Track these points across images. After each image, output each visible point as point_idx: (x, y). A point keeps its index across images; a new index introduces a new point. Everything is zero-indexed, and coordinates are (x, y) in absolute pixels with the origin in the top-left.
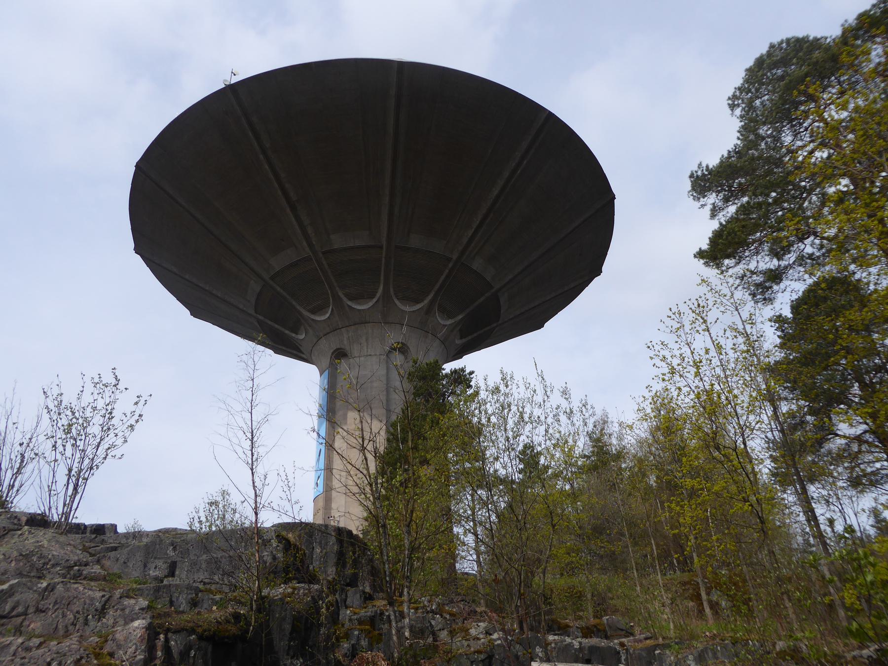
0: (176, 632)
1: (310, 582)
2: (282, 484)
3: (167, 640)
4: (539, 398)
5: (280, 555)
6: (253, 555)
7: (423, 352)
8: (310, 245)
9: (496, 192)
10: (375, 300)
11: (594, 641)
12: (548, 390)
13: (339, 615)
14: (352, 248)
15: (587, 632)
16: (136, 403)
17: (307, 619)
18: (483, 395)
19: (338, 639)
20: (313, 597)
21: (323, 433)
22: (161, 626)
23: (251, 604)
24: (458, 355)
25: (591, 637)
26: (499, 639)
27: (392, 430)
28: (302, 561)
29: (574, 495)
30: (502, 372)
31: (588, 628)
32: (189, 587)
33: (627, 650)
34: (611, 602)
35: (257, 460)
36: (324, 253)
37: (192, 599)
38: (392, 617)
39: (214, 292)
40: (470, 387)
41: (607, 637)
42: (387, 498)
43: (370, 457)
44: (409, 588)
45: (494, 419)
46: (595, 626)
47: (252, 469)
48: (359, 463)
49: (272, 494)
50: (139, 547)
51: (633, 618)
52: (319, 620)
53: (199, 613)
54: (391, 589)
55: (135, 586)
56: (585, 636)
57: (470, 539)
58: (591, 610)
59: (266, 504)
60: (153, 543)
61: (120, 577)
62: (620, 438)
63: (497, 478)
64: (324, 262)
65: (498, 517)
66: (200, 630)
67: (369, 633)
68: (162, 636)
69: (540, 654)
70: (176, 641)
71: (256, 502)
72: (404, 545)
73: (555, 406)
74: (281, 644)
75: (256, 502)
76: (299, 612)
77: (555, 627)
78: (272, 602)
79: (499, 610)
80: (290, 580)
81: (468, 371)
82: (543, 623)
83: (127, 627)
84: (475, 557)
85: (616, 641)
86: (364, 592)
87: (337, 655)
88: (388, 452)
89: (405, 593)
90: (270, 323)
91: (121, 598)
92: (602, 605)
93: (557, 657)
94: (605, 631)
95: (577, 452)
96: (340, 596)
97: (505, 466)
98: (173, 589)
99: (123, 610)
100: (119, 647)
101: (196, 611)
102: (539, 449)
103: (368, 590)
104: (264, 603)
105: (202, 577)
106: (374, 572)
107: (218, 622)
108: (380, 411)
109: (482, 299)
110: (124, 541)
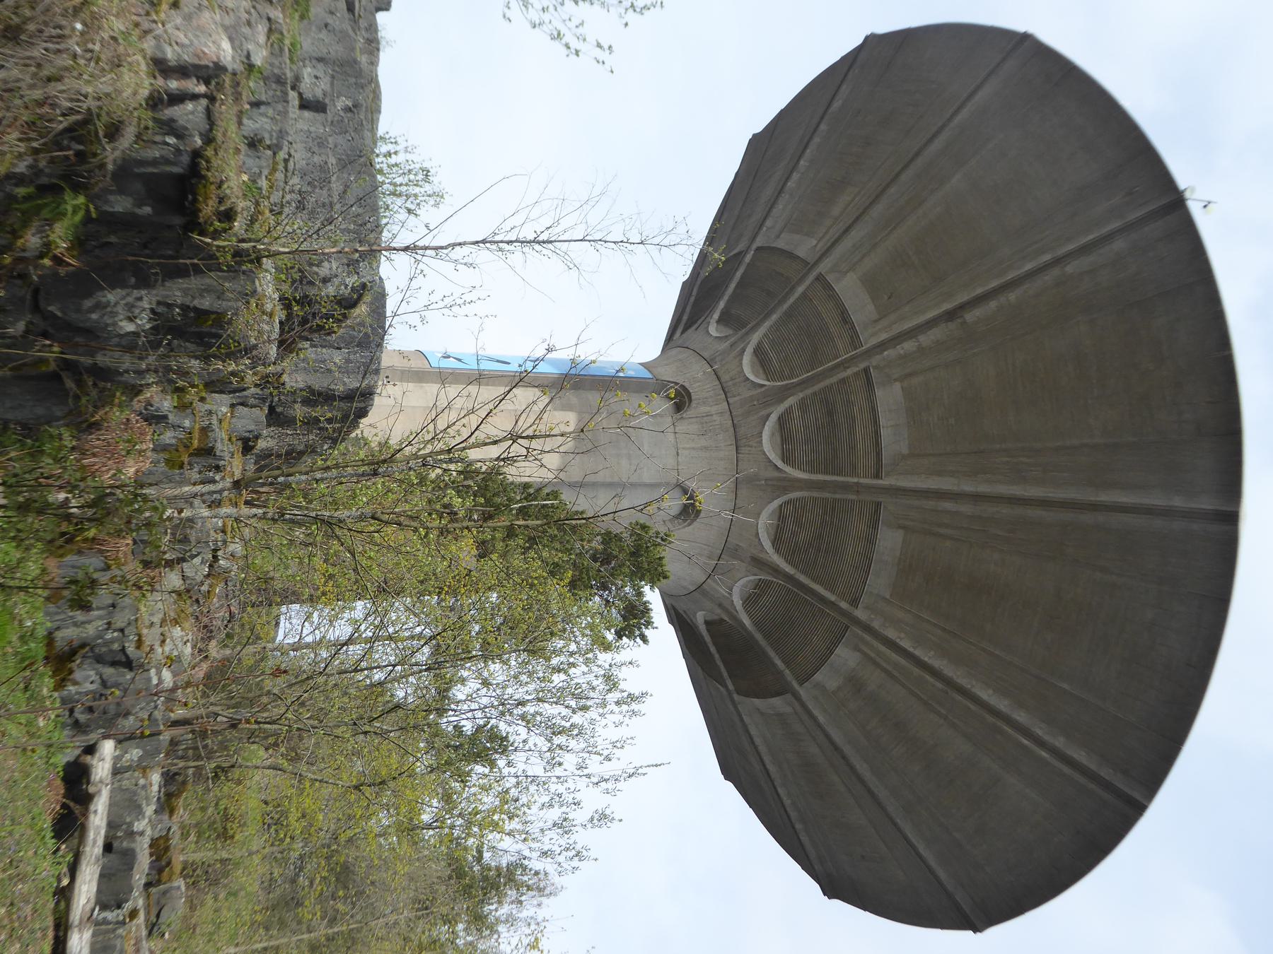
0: (209, 113)
1: (281, 343)
2: (456, 295)
3: (195, 97)
4: (594, 765)
5: (331, 290)
6: (335, 244)
7: (684, 556)
8: (882, 346)
9: (985, 694)
10: (779, 464)
11: (144, 860)
12: (610, 785)
13: (221, 392)
15: (160, 848)
16: (599, 46)
17: (219, 336)
18: (604, 658)
19: (180, 390)
20: (255, 347)
21: (543, 368)
22: (220, 87)
23: (250, 240)
24: (678, 618)
25: (151, 855)
26: (160, 681)
27: (546, 491)
28: (320, 328)
29: (410, 829)
30: (644, 695)
31: (167, 849)
32: (282, 134)
33: (123, 923)
34: (210, 896)
35: (501, 250)
36: (866, 371)
37: (261, 141)
38: (212, 487)
39: (795, 176)
40: (619, 635)
41: (148, 885)
42: (423, 480)
43: (494, 452)
44: (263, 517)
45: (558, 679)
46: (169, 863)
47: (484, 242)
48: (488, 432)
49: (439, 277)
50: (353, 49)
51: (178, 939)
52: (215, 357)
53: (238, 151)
54: (263, 485)
55: (287, 42)
56: (154, 843)
57: (342, 630)
58: (197, 857)
59: (421, 266)
60: (359, 74)
61: (302, 17)
62: (510, 920)
63: (450, 683)
64: (849, 372)
65: (381, 684)
66: (209, 152)
67: (186, 447)
68: (202, 89)
69: (128, 756)
70: (192, 113)
71: (426, 248)
73: (578, 796)
74: (176, 292)
75: (426, 248)
76: (230, 322)
77: (173, 788)
78: (250, 276)
79: (213, 681)
80: (288, 307)
81: (647, 632)
82: (181, 764)
83: (220, 30)
84: (309, 639)
85: (141, 902)
86: (257, 438)
87: (154, 388)
88: (505, 487)
89: (254, 511)
90: (739, 274)
91: (269, 19)
92: (205, 878)
93: (121, 789)
94: (159, 882)
95: (492, 836)
96: (253, 396)
97: (470, 698)
98: (280, 107)
99: (249, 23)
100: (188, 18)
101: (243, 147)
102: (501, 763)
103: (261, 444)
104: (251, 262)
105: (297, 156)
106: (293, 456)
107: (222, 182)
108: (575, 474)
109: (778, 662)
110: (363, 23)
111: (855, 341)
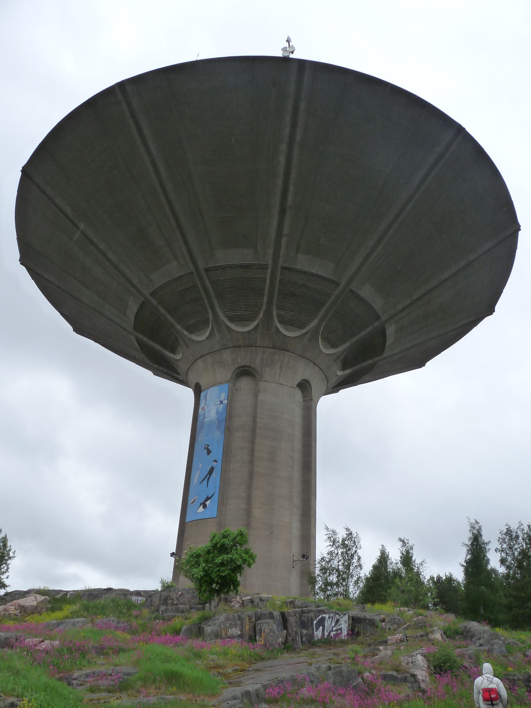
8: (276, 254)
10: (303, 331)
14: (313, 275)
39: (110, 254)
72: (341, 629)
111: (264, 268)
